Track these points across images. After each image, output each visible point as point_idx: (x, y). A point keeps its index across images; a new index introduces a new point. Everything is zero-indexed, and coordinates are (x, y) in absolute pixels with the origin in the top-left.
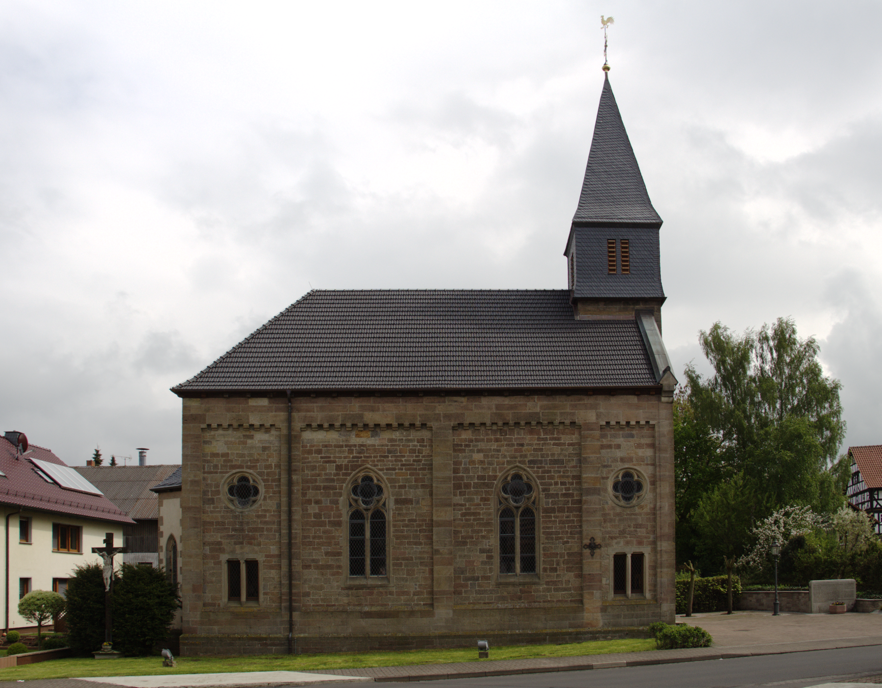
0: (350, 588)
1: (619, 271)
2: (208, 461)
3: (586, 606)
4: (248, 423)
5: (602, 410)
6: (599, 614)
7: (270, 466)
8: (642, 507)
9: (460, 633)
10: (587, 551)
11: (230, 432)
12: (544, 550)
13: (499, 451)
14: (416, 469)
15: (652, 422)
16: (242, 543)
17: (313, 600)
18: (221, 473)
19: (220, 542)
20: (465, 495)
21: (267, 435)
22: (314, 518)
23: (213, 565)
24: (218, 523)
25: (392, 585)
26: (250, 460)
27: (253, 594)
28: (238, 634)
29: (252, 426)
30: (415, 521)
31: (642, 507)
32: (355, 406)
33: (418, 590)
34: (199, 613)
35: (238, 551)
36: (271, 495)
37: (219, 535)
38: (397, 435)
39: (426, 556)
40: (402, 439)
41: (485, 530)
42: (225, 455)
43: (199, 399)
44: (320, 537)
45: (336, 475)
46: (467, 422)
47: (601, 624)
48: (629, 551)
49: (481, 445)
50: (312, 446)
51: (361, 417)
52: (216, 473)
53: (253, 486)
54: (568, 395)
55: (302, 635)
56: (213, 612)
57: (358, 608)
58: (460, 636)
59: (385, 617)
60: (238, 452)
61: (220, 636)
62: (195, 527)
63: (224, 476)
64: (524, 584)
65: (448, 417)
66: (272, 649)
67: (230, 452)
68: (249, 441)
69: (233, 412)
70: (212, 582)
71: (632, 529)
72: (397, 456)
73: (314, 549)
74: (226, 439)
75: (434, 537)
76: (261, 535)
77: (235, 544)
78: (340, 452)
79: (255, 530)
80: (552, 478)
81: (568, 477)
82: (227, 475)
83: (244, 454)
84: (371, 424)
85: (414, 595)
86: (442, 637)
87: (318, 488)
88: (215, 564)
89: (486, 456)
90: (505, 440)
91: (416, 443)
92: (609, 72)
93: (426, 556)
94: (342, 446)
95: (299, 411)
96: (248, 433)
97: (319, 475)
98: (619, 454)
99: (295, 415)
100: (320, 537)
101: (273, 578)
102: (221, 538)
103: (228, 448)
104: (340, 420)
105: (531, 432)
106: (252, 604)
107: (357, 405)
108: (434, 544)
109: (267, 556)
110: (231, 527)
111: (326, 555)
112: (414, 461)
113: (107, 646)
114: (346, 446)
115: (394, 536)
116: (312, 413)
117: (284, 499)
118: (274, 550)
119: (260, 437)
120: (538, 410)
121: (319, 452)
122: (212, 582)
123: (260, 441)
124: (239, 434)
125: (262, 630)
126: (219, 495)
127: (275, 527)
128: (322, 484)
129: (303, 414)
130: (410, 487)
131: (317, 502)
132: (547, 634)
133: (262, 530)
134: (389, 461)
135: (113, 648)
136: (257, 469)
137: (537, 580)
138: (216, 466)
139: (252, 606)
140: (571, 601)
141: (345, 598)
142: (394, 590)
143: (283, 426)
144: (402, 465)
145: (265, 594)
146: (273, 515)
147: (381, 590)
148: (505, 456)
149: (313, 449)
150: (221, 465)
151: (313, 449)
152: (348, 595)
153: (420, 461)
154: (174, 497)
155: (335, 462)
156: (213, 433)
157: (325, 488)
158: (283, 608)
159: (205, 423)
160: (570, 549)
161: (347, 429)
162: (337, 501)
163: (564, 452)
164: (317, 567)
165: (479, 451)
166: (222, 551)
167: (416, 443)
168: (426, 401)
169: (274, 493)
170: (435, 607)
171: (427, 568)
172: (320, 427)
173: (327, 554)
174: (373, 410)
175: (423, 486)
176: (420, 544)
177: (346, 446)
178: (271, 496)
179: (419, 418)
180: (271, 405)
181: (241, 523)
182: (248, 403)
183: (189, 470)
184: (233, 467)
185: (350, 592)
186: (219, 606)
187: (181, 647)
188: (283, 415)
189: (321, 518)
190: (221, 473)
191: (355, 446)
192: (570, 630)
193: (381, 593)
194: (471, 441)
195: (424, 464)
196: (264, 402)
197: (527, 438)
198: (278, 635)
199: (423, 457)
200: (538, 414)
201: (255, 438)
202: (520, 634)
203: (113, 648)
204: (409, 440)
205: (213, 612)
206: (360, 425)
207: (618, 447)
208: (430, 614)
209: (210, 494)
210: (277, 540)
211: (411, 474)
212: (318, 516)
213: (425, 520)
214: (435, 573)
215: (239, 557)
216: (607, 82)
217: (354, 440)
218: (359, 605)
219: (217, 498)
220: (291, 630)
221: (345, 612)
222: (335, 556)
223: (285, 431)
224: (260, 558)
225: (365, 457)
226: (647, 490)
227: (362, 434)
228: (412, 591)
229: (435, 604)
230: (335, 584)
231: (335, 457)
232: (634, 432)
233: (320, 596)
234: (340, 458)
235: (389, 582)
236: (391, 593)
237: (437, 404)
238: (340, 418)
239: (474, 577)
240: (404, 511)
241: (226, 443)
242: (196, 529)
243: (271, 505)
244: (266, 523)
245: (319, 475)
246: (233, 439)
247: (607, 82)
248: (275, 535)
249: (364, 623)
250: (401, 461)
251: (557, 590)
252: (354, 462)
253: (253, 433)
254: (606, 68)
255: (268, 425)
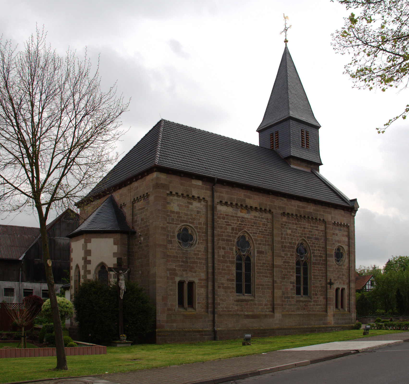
0: (238, 301)
1: (305, 147)
2: (168, 216)
3: (328, 314)
4: (192, 194)
5: (333, 215)
6: (332, 318)
7: (200, 224)
8: (344, 266)
9: (285, 327)
10: (328, 286)
11: (181, 198)
12: (313, 284)
13: (296, 230)
14: (265, 235)
15: (348, 225)
16: (186, 271)
17: (221, 307)
18: (176, 224)
19: (175, 269)
20: (284, 252)
21: (199, 204)
22: (222, 258)
23: (171, 284)
24: (174, 257)
25: (256, 299)
26: (191, 218)
27: (191, 303)
28: (186, 328)
29: (193, 196)
30: (265, 264)
31: (344, 266)
32: (241, 194)
33: (266, 303)
34: (166, 315)
35: (185, 276)
36: (201, 241)
37: (174, 264)
38: (257, 214)
39: (270, 284)
40: (259, 217)
41: (292, 272)
42: (178, 213)
43: (166, 174)
44: (225, 270)
45: (232, 233)
46: (286, 212)
47: (333, 323)
48: (341, 287)
49: (290, 226)
50: (221, 214)
51: (244, 201)
52: (173, 224)
53: (190, 235)
54: (322, 205)
55: (219, 329)
56: (174, 314)
57: (242, 313)
58: (285, 329)
59: (255, 318)
60: (184, 212)
61: (178, 330)
62: (163, 258)
63: (177, 226)
64: (305, 301)
65: (279, 207)
66: (205, 337)
67: (180, 211)
68: (190, 206)
69: (184, 186)
70: (171, 295)
71: (341, 276)
72: (257, 226)
73: (222, 276)
74: (179, 203)
75: (275, 273)
76: (196, 266)
77: (183, 270)
78: (234, 220)
79: (194, 262)
80: (315, 247)
81: (320, 247)
82: (179, 226)
83: (188, 214)
84: (249, 206)
85: (265, 306)
86: (279, 329)
87: (223, 240)
88: (172, 283)
89: (292, 232)
90: (299, 224)
91: (265, 220)
92: (287, 43)
93: (270, 284)
94: (233, 217)
95: (217, 192)
96: (189, 201)
97: (224, 232)
98: (337, 238)
99: (215, 194)
100: (225, 270)
101: (203, 293)
102: (175, 266)
103: (180, 209)
104: (235, 201)
105: (308, 222)
106: (190, 309)
107: (243, 194)
108: (274, 277)
109: (199, 280)
110: (181, 260)
111: (227, 281)
112: (265, 230)
113: (124, 337)
114: (236, 217)
115: (256, 271)
116: (223, 194)
117: (210, 245)
118: (203, 276)
119: (196, 205)
120: (312, 211)
121: (224, 218)
122: (171, 295)
123: (196, 207)
124: (186, 201)
125: (199, 325)
126: (174, 238)
127: (204, 261)
128: (225, 238)
129: (218, 194)
130: (263, 244)
131: (224, 248)
132: (316, 328)
133: (196, 263)
134: (254, 228)
135: (127, 339)
136: (194, 225)
137: (310, 300)
138: (173, 219)
139: (190, 311)
140: (322, 311)
141: (236, 307)
142: (256, 302)
143: (209, 199)
144: (260, 232)
145: (199, 303)
146: (202, 254)
147: (252, 302)
148: (299, 233)
149: (221, 216)
150: (176, 219)
151: (221, 216)
152: (237, 305)
153: (266, 230)
154: (110, 238)
155: (231, 226)
156: (171, 197)
157: (227, 240)
158: (209, 312)
159: (169, 190)
160: (321, 284)
161: (238, 207)
162: (233, 248)
163: (319, 234)
164: (224, 288)
165: (290, 229)
166: (176, 275)
167: (265, 220)
168: (271, 197)
169: (203, 240)
170: (275, 313)
171: (270, 291)
172: (226, 203)
173: (228, 280)
174: (250, 198)
175: (268, 245)
176: (267, 277)
177: (236, 217)
178: (201, 242)
179: (268, 207)
180: (203, 186)
181: (186, 258)
182: (191, 182)
183: (160, 220)
184: (182, 221)
185: (238, 303)
186: (174, 310)
187: (157, 337)
188: (209, 193)
189: (225, 258)
190: (176, 224)
191: (240, 217)
192: (324, 326)
193: (251, 304)
194: (286, 223)
195: (268, 233)
196: (199, 183)
197: (307, 225)
198: (207, 329)
199: (268, 228)
200: (312, 213)
201: (193, 205)
202: (307, 328)
203: (127, 339)
204: (262, 218)
205: (174, 314)
206: (244, 205)
207: (337, 235)
208: (272, 317)
209: (169, 237)
210: (204, 270)
211: (264, 237)
212: (224, 257)
213: (269, 264)
214: (275, 293)
215: (185, 279)
216: (286, 48)
217: (240, 214)
218: (242, 311)
219: (174, 240)
220: (214, 326)
221: (237, 315)
222: (231, 281)
223: (210, 203)
224: (196, 280)
225: (244, 224)
226: (345, 258)
227: (243, 211)
228: (264, 303)
229: (275, 311)
230: (232, 298)
231: (231, 223)
232: (342, 228)
233: (225, 305)
234: (233, 223)
235: (255, 298)
236: (255, 304)
237: (275, 200)
238: (235, 200)
239: (288, 296)
240: (261, 258)
241: (178, 205)
242: (164, 260)
243: (202, 247)
244: (199, 259)
245: (224, 232)
246: (182, 204)
247: (286, 48)
248: (203, 267)
249: (246, 321)
250: (259, 229)
251: (317, 305)
252: (239, 226)
253: (192, 201)
254: (286, 41)
255: (201, 197)
